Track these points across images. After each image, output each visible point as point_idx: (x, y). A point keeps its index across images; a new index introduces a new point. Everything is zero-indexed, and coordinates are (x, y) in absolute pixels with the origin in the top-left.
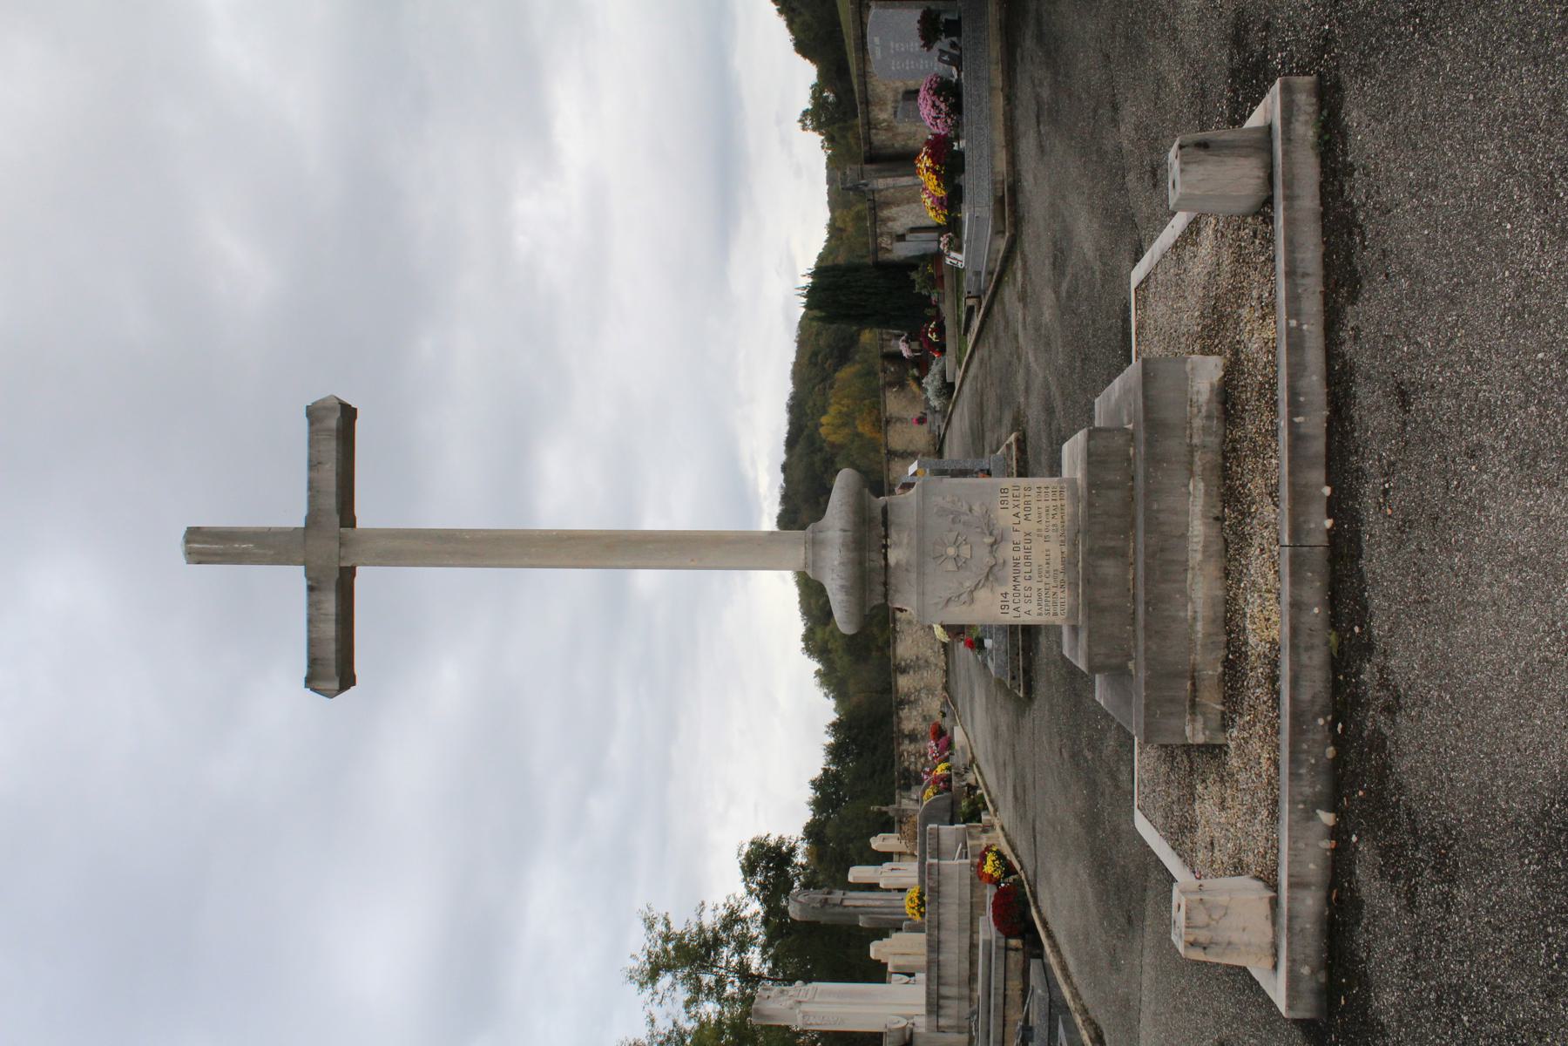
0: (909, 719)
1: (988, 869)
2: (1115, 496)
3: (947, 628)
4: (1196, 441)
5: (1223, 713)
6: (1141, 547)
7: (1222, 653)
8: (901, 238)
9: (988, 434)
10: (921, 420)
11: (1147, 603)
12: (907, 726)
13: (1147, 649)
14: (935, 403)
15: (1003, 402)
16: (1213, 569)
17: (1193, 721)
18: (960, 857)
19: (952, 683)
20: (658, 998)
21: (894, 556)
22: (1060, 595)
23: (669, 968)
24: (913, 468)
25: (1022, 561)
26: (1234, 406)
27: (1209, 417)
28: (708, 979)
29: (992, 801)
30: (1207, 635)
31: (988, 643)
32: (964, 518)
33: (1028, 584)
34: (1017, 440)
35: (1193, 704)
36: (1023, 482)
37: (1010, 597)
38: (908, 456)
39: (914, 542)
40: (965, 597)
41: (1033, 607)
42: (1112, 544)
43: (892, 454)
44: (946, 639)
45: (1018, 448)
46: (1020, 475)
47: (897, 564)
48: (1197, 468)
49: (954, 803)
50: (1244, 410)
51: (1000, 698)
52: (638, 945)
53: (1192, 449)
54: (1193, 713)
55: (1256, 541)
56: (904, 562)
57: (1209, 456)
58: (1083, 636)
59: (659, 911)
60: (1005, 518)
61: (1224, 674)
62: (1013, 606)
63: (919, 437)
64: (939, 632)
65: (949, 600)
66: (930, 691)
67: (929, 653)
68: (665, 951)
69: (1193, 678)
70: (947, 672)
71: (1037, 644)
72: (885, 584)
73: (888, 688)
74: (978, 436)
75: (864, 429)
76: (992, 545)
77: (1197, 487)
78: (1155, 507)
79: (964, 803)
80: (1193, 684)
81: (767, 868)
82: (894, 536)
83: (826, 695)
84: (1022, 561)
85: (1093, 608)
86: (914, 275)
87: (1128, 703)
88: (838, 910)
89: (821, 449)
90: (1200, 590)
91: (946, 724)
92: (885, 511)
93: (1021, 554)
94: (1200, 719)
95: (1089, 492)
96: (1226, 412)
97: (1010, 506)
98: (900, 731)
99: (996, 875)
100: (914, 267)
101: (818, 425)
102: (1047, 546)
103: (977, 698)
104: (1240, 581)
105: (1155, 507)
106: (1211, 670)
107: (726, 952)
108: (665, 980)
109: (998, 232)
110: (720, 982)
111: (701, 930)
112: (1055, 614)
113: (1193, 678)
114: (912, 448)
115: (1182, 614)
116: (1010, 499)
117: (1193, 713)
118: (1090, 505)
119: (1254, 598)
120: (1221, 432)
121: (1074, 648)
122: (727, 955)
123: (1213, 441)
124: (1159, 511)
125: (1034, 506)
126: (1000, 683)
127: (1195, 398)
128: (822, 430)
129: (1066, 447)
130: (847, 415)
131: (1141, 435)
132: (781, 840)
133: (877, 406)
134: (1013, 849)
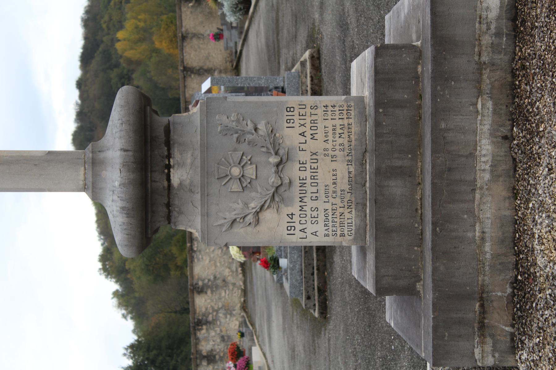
0: (206, 339)
2: (403, 114)
3: (243, 249)
4: (485, 58)
5: (512, 335)
6: (428, 167)
7: (511, 274)
9: (284, 51)
10: (218, 37)
11: (434, 224)
12: (205, 347)
13: (435, 270)
14: (231, 18)
15: (297, 18)
16: (501, 189)
17: (482, 343)
19: (250, 304)
21: (176, 177)
22: (347, 215)
24: (206, 85)
25: (309, 181)
26: (524, 22)
27: (498, 34)
30: (495, 256)
31: (283, 262)
32: (249, 137)
33: (314, 204)
34: (312, 57)
35: (482, 326)
36: (309, 99)
37: (296, 218)
38: (203, 72)
39: (198, 162)
41: (320, 228)
42: (398, 163)
43: (188, 71)
44: (242, 259)
45: (313, 65)
46: (315, 93)
47: (181, 184)
48: (486, 85)
50: (533, 27)
51: (297, 318)
53: (481, 66)
54: (482, 336)
55: (545, 160)
57: (498, 74)
58: (371, 257)
60: (291, 137)
61: (513, 295)
62: (299, 227)
63: (216, 53)
64: (234, 251)
66: (229, 311)
67: (227, 272)
69: (481, 299)
70: (245, 292)
71: (332, 263)
72: (168, 205)
73: (186, 309)
74: (273, 54)
75: (162, 45)
76: (278, 165)
77: (486, 106)
78: (443, 125)
80: (482, 306)
82: (177, 155)
83: (124, 316)
84: (309, 181)
85: (382, 229)
87: (418, 325)
89: (117, 65)
90: (488, 210)
91: (244, 344)
92: (168, 130)
93: (308, 174)
94: (489, 340)
95: (376, 112)
96: (515, 28)
97: (296, 124)
98: (198, 352)
101: (114, 40)
102: (334, 165)
103: (274, 318)
104: (528, 201)
105: (443, 125)
106: (500, 291)
112: (342, 235)
113: (481, 299)
114: (208, 65)
115: (470, 235)
116: (296, 118)
117: (482, 336)
118: (377, 124)
119: (542, 219)
120: (510, 49)
121: (362, 269)
123: (502, 59)
124: (447, 130)
125: (321, 125)
126: (296, 303)
127: (484, 14)
128: (119, 46)
129: (354, 65)
130: (145, 30)
131: (428, 53)
133: (174, 21)
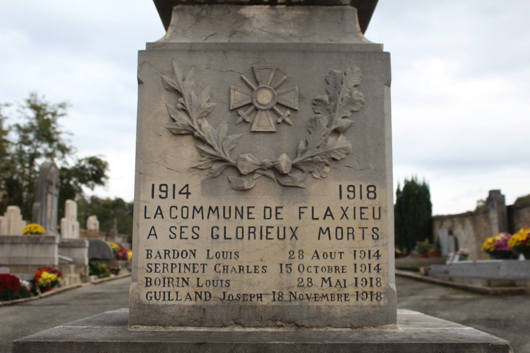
1: (46, 275)
8: (451, 233)
18: (60, 259)
20: (21, 109)
22: (183, 291)
23: (38, 116)
28: (31, 136)
29: (102, 282)
32: (324, 120)
33: (205, 233)
40: (183, 119)
41: (162, 243)
47: (245, 19)
49: (106, 260)
52: (50, 98)
56: (247, 28)
59: (69, 111)
62: (165, 205)
65: (179, 93)
68: (46, 114)
76: (275, 169)
79: (104, 265)
81: (92, 170)
84: (246, 223)
86: (427, 241)
88: (45, 190)
93: (259, 221)
97: (345, 203)
99: (40, 280)
100: (431, 241)
102: (273, 269)
107: (46, 146)
108: (32, 114)
109: (489, 282)
110: (29, 143)
111: (58, 133)
112: (148, 282)
116: (357, 202)
122: (43, 147)
125: (345, 245)
132: (107, 178)
134: (59, 293)
